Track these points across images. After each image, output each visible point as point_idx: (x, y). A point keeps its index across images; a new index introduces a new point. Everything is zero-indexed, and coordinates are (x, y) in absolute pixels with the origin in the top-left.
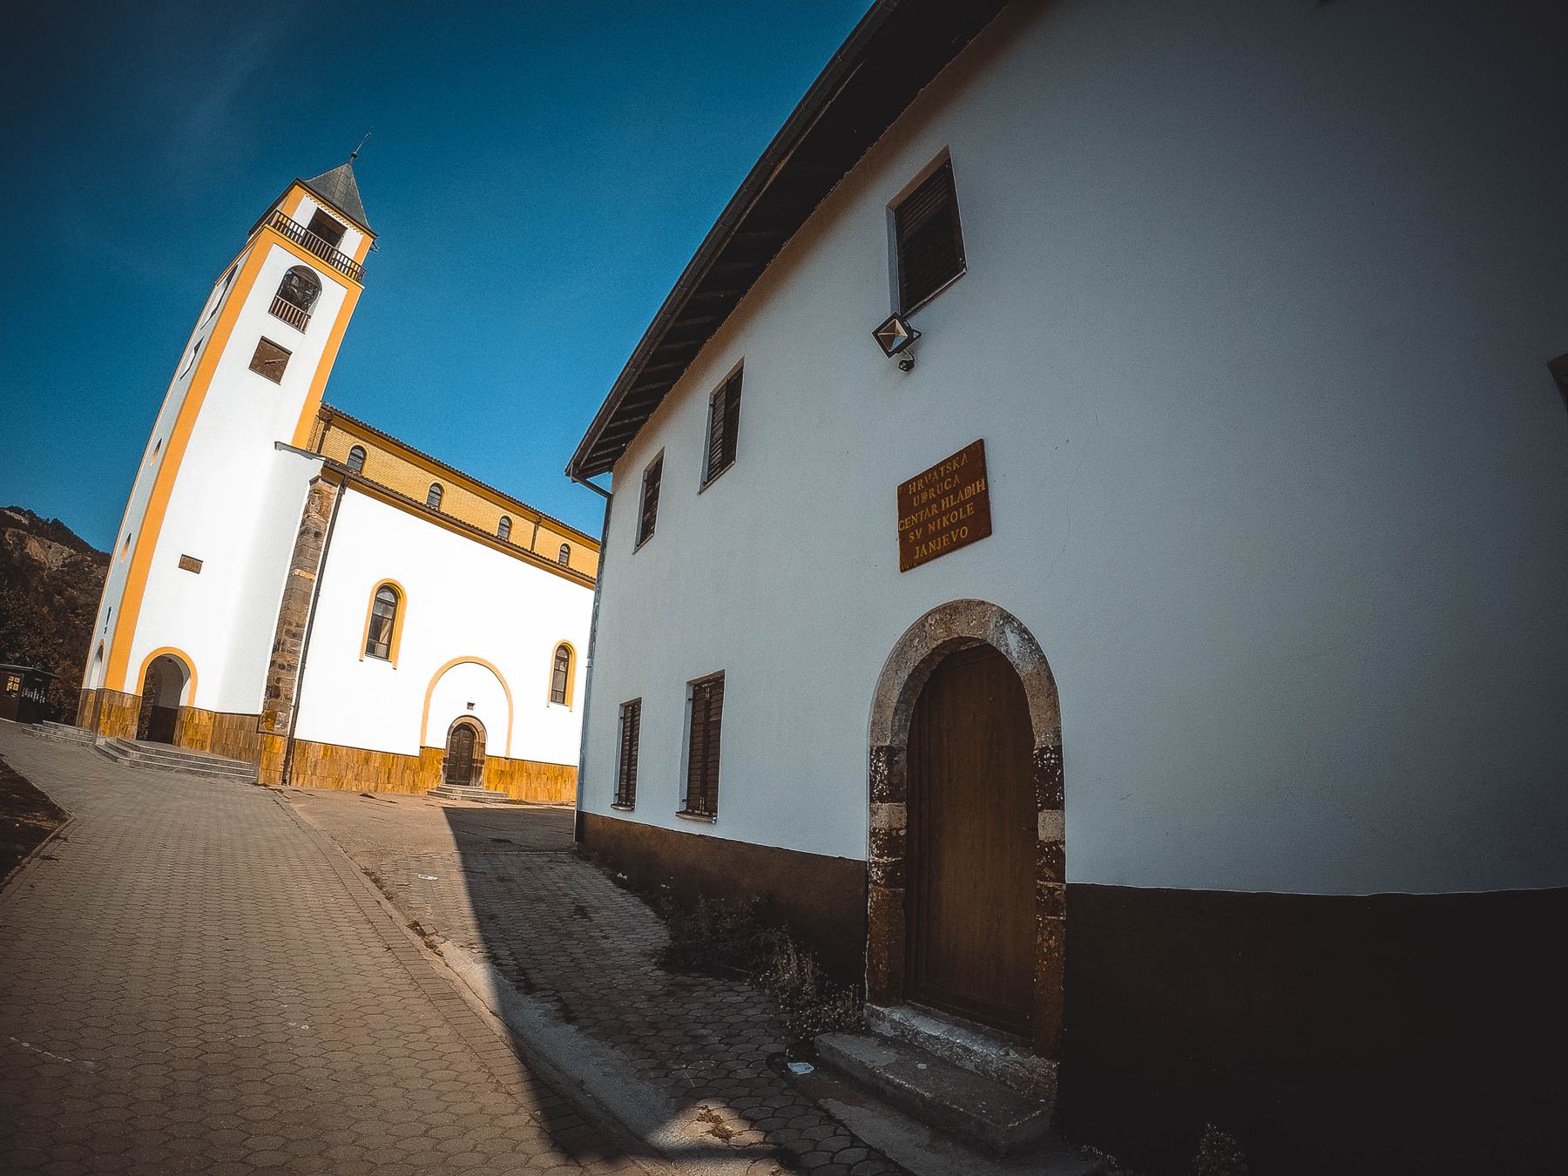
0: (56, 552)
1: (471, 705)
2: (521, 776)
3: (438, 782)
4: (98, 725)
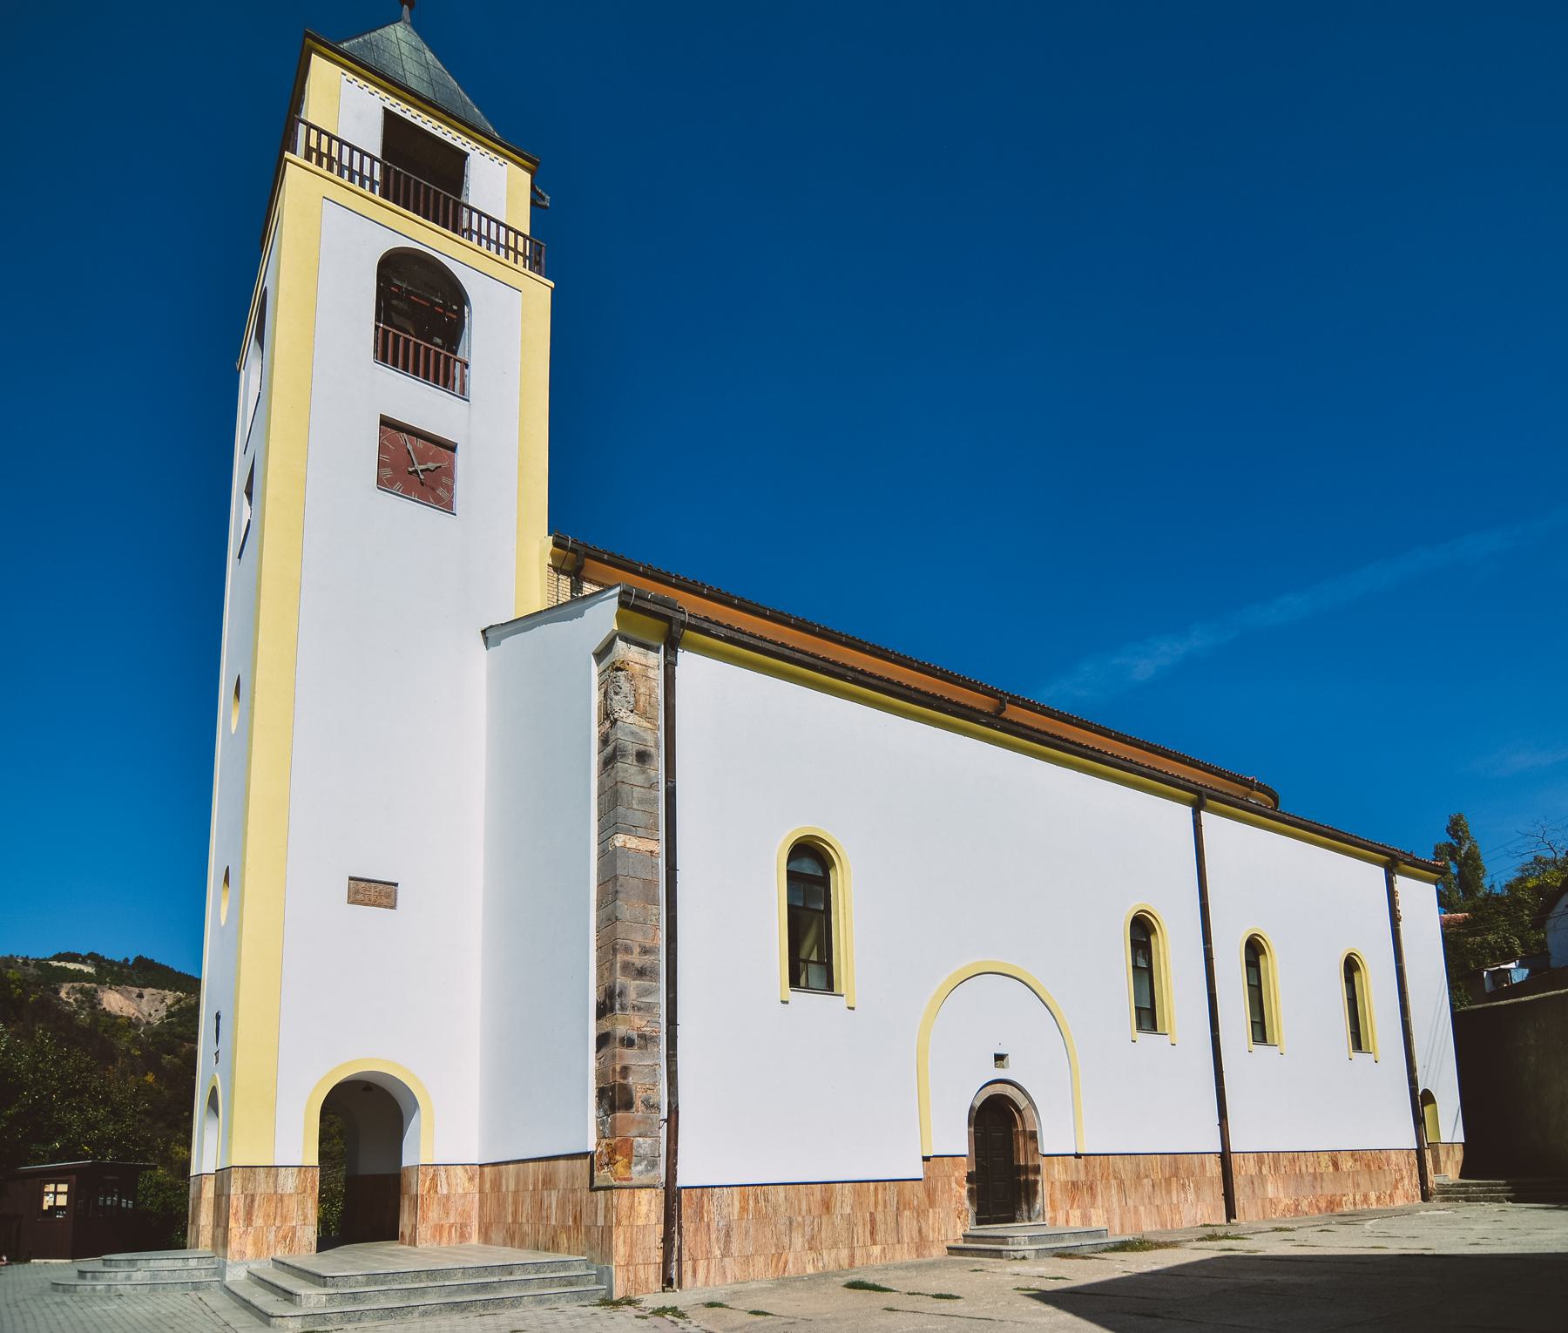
0: (154, 1001)
1: (999, 1058)
2: (1108, 1187)
3: (964, 1225)
4: (225, 1243)
